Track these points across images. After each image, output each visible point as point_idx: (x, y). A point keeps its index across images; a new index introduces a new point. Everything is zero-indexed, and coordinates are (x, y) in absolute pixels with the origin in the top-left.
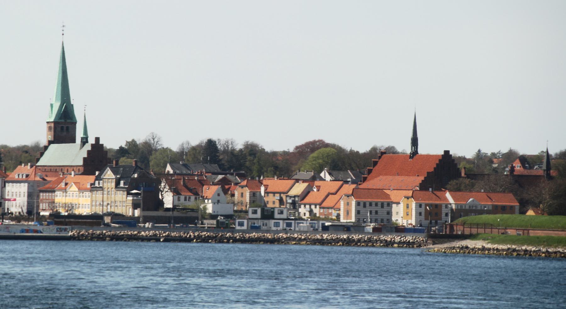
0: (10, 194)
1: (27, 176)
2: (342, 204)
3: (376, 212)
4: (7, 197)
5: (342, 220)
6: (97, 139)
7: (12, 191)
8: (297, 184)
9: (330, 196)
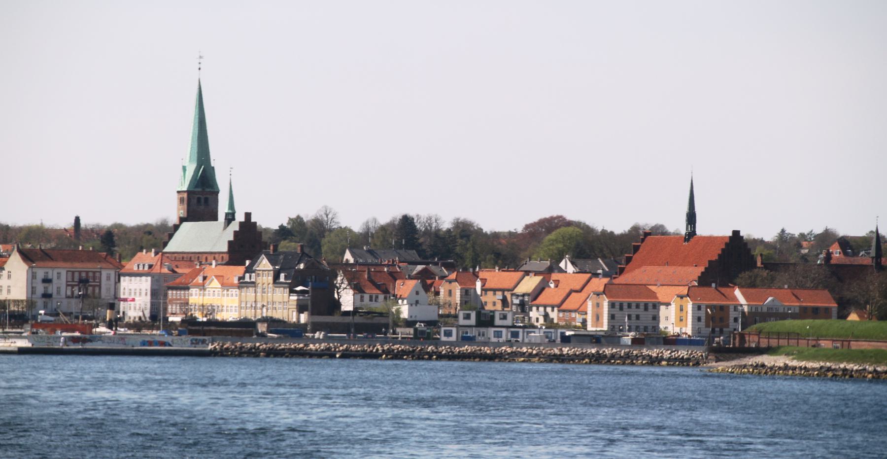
0: (127, 292)
1: (150, 266)
3: (638, 317)
4: (122, 296)
5: (590, 328)
6: (248, 215)
7: (130, 288)
8: (527, 278)
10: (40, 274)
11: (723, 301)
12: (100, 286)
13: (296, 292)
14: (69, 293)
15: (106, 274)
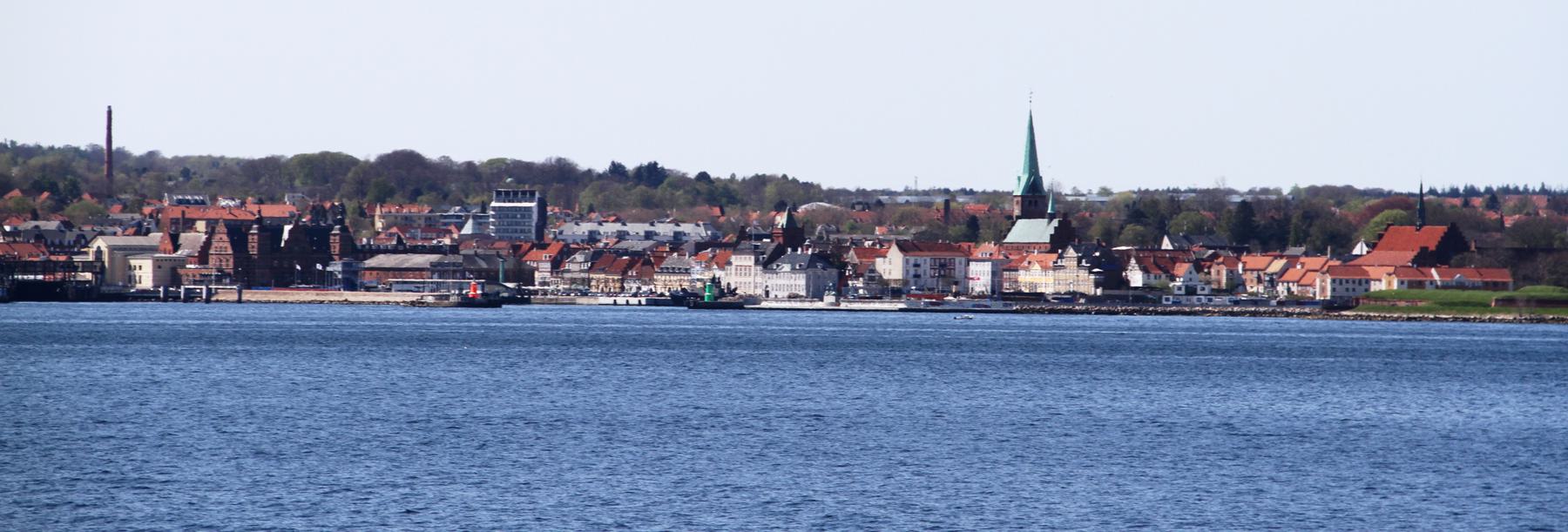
0: (974, 272)
1: (991, 254)
2: (1318, 282)
3: (1354, 290)
4: (971, 276)
5: (1318, 298)
9: (1309, 273)
10: (912, 260)
11: (1418, 277)
12: (954, 269)
13: (1093, 273)
14: (932, 273)
15: (959, 260)
